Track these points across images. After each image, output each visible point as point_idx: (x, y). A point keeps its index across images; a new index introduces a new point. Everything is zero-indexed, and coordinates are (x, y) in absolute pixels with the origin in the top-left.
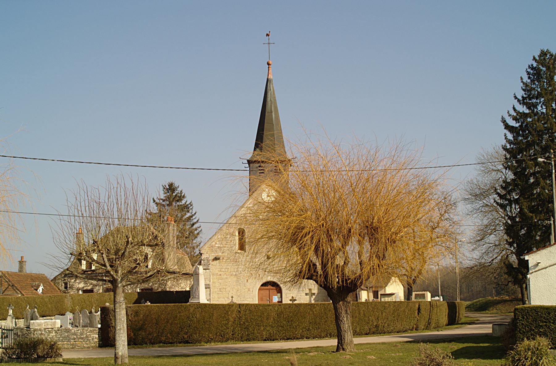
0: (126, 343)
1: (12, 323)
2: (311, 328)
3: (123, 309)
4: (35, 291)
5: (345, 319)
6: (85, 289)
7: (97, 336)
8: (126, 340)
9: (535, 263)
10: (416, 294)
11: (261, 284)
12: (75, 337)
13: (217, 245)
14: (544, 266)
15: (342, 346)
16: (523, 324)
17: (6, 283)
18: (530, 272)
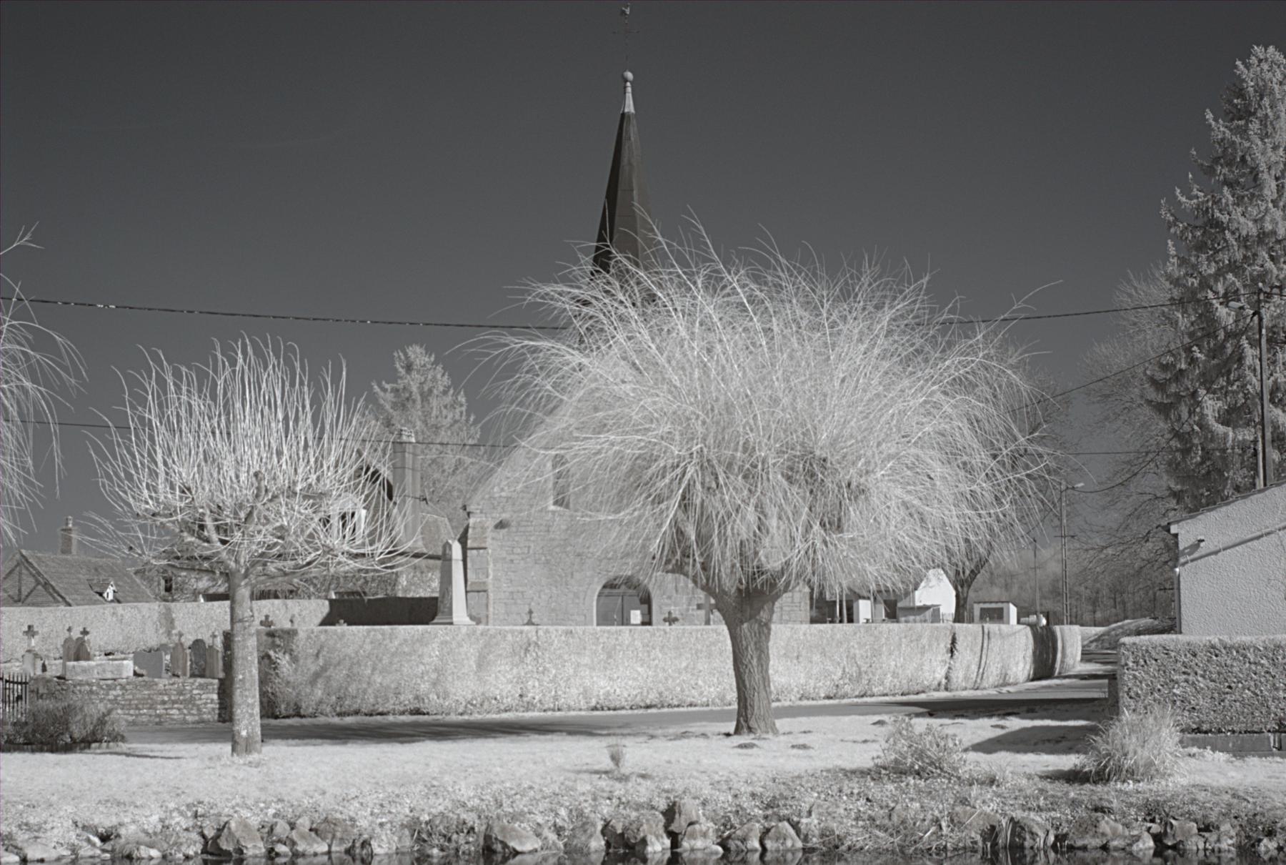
0: (257, 710)
1: (35, 669)
2: (700, 683)
3: (251, 635)
4: (98, 597)
5: (755, 662)
6: (211, 591)
7: (215, 697)
8: (257, 703)
9: (1192, 541)
10: (982, 609)
11: (604, 582)
12: (166, 698)
13: (503, 494)
14: (1212, 549)
15: (746, 721)
16: (1135, 677)
17: (32, 580)
18: (1182, 560)
